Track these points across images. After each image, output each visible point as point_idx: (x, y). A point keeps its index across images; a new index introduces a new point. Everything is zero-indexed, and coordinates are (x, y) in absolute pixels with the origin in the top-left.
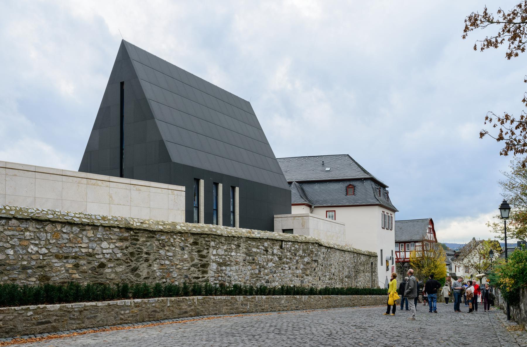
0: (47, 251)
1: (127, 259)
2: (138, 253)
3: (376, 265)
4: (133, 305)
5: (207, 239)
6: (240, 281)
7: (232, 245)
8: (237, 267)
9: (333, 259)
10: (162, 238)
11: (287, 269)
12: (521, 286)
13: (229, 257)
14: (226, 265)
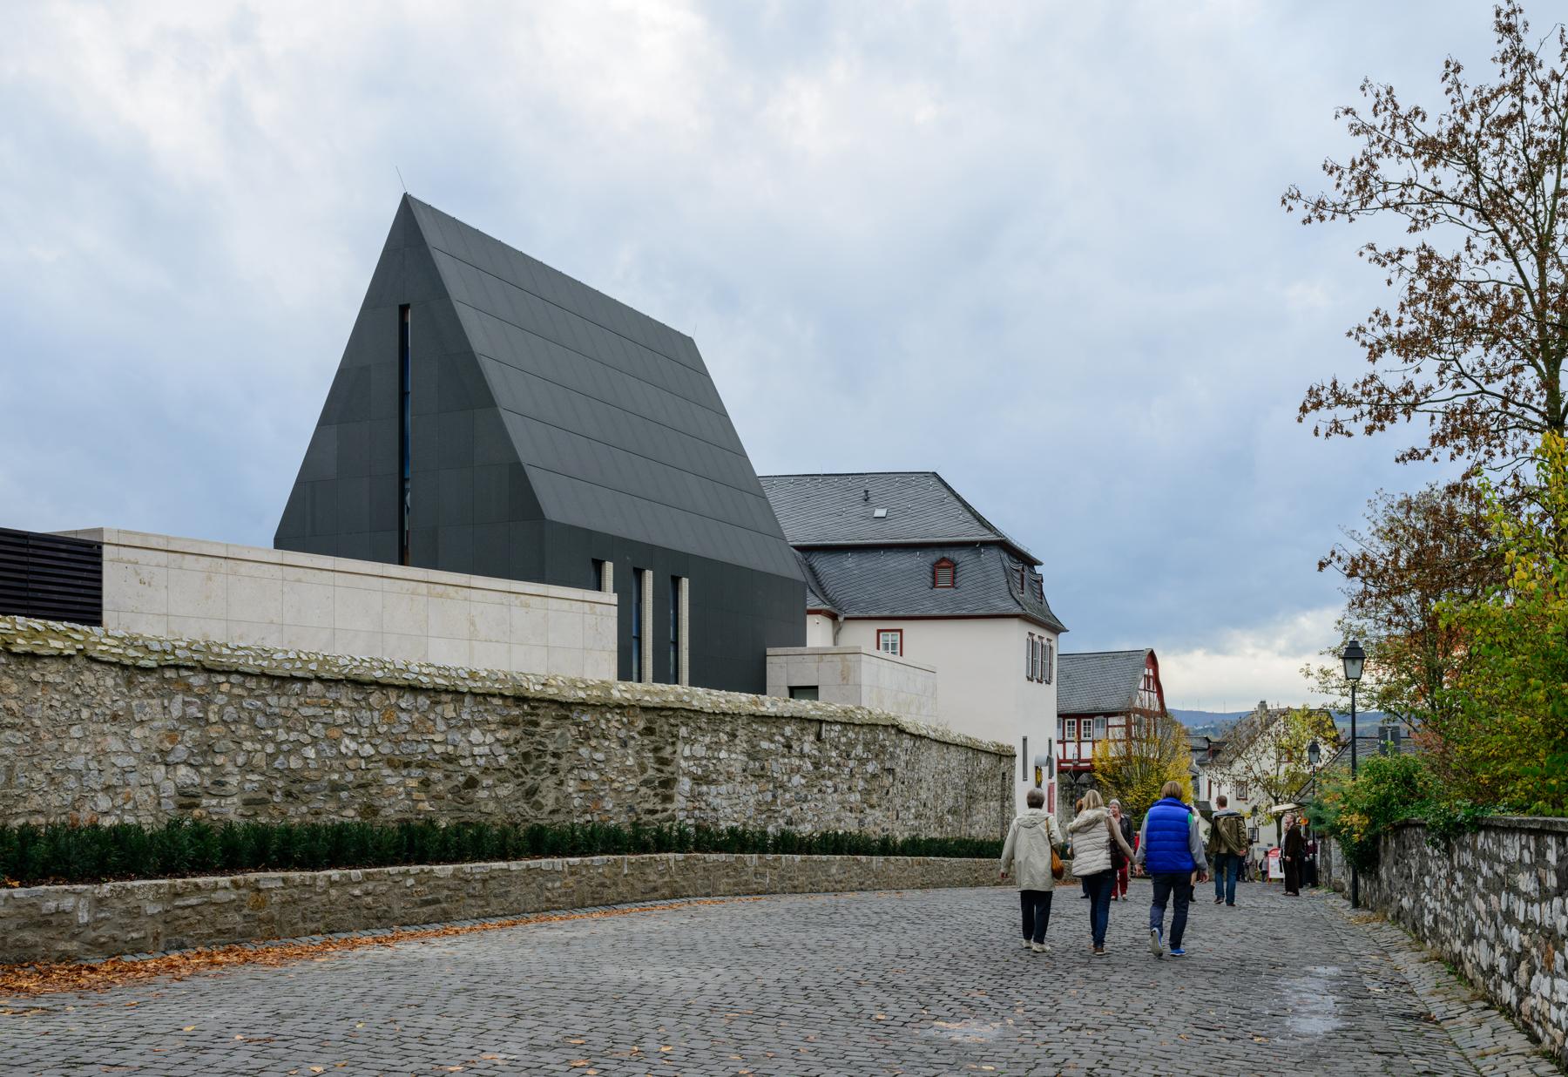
0: (373, 752)
1: (517, 769)
2: (537, 753)
3: (1012, 778)
4: (566, 870)
5: (672, 721)
6: (735, 821)
7: (721, 734)
8: (730, 785)
9: (924, 764)
10: (585, 718)
11: (829, 791)
12: (1381, 829)
13: (714, 761)
14: (709, 783)
